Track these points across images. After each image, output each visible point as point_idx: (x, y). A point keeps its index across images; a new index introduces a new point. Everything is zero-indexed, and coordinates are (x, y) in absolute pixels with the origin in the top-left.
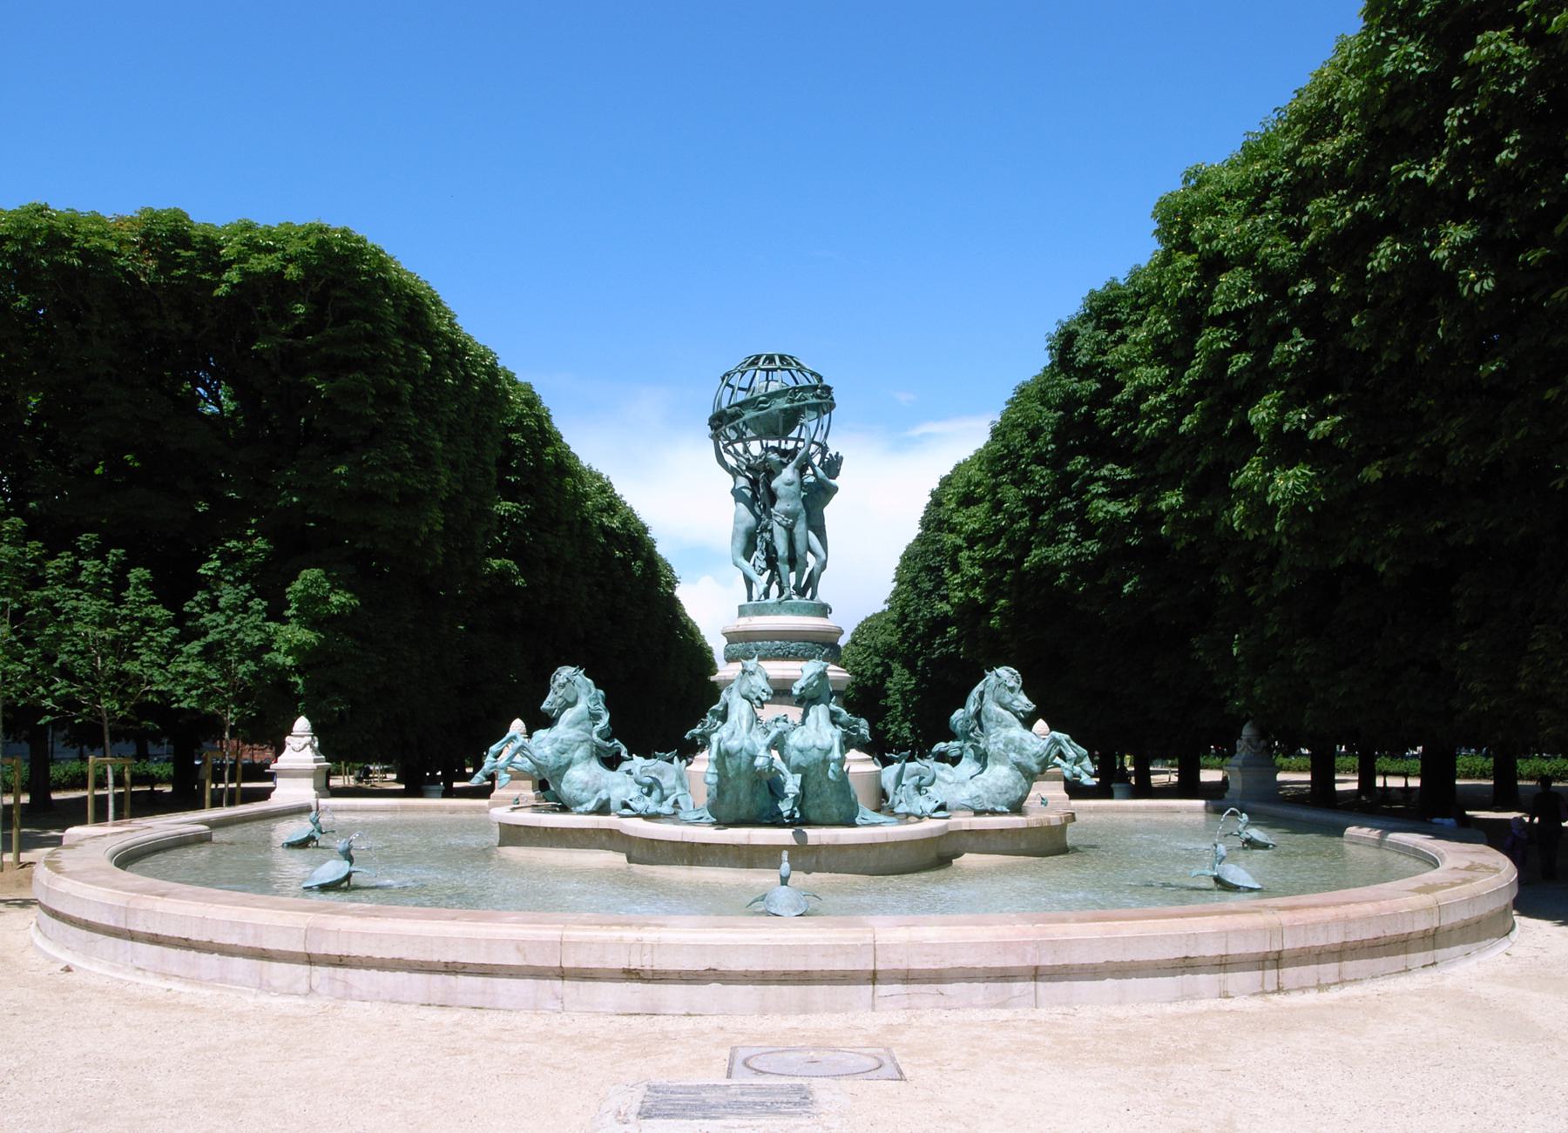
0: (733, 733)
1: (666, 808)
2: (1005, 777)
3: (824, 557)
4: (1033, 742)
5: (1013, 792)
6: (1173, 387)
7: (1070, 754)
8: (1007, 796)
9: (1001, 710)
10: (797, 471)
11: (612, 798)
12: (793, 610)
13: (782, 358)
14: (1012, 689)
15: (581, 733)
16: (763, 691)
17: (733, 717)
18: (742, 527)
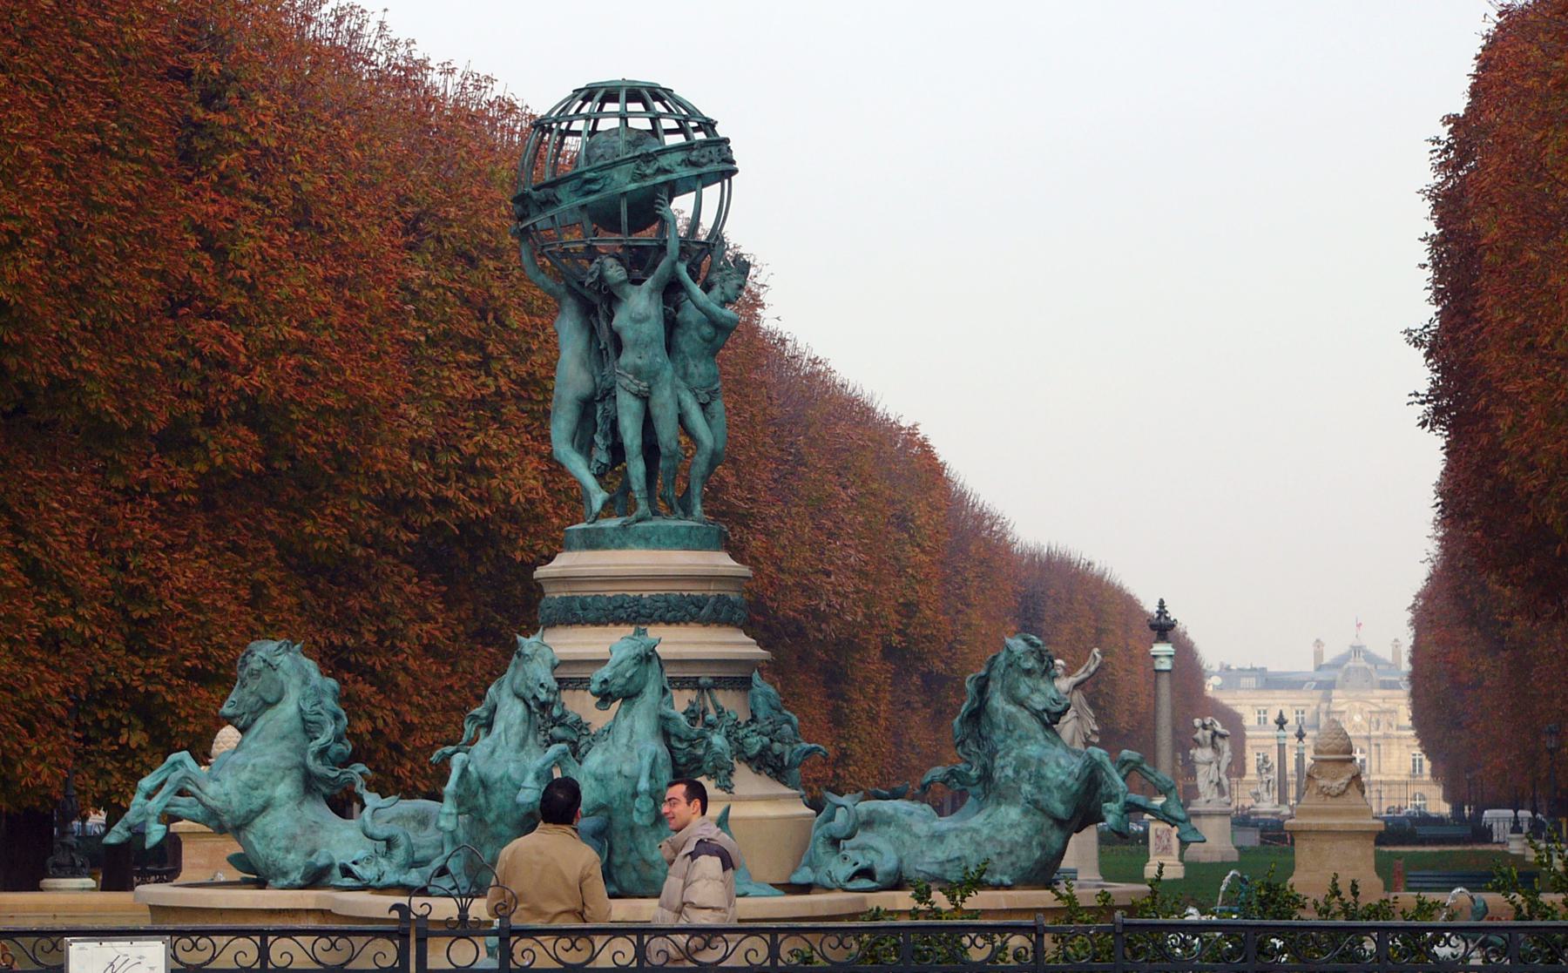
0: (493, 752)
6: (404, 323)
8: (1013, 858)
9: (1012, 709)
10: (655, 296)
15: (287, 754)
17: (499, 727)
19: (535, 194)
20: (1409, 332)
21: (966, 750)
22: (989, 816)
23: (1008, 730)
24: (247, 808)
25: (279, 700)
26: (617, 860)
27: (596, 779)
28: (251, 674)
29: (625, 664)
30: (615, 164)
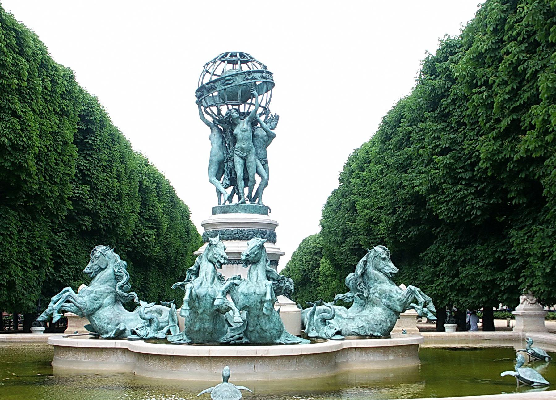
0: (201, 284)
1: (161, 335)
2: (379, 315)
3: (266, 177)
4: (397, 292)
5: (385, 324)
7: (421, 300)
8: (381, 326)
9: (377, 272)
10: (249, 123)
11: (127, 328)
12: (246, 210)
13: (242, 55)
14: (384, 259)
15: (109, 287)
16: (222, 257)
17: (202, 274)
18: (215, 159)
19: (207, 86)
20: (277, 225)
21: (361, 287)
22: (370, 311)
23: (375, 280)
24: (93, 308)
25: (106, 268)
26: (250, 329)
27: (244, 295)
28: (95, 258)
29: (254, 249)
30: (237, 75)
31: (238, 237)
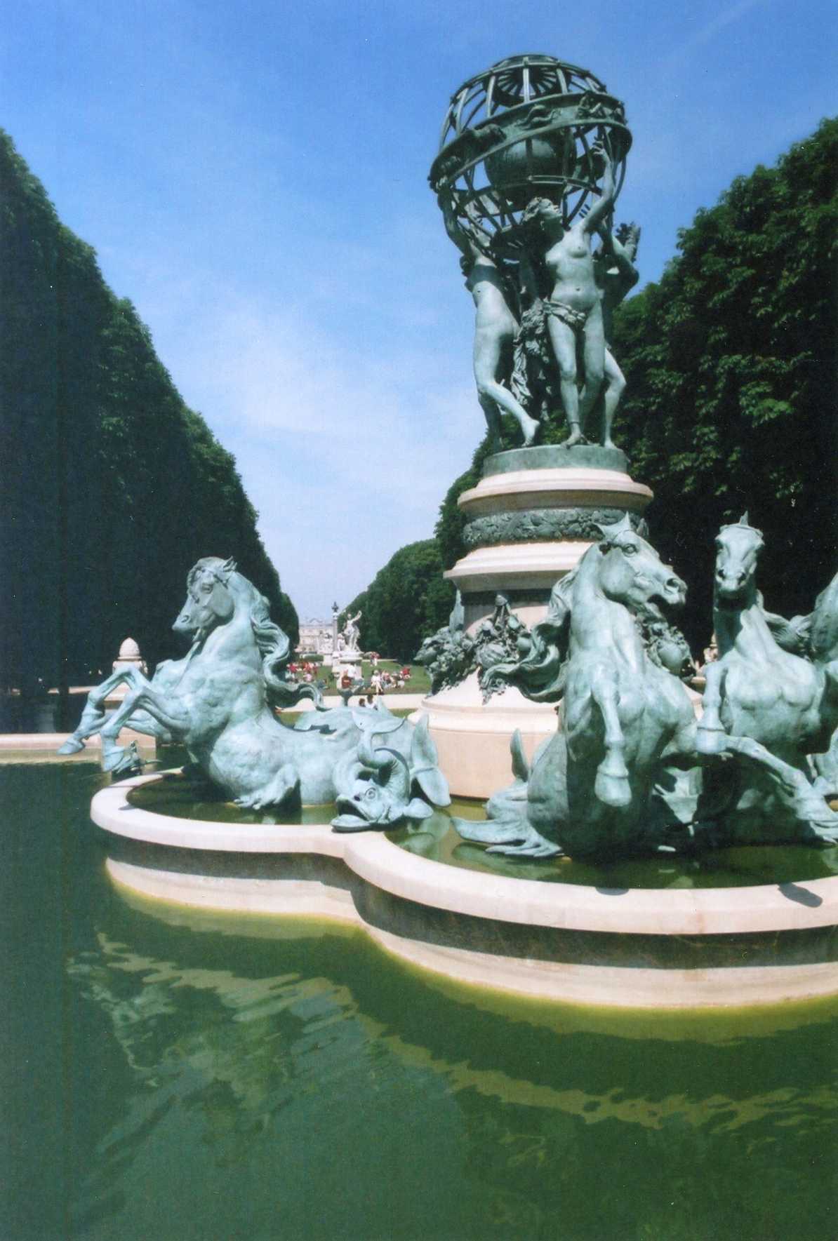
11: (303, 778)
15: (243, 667)
19: (478, 133)
31: (580, 530)
